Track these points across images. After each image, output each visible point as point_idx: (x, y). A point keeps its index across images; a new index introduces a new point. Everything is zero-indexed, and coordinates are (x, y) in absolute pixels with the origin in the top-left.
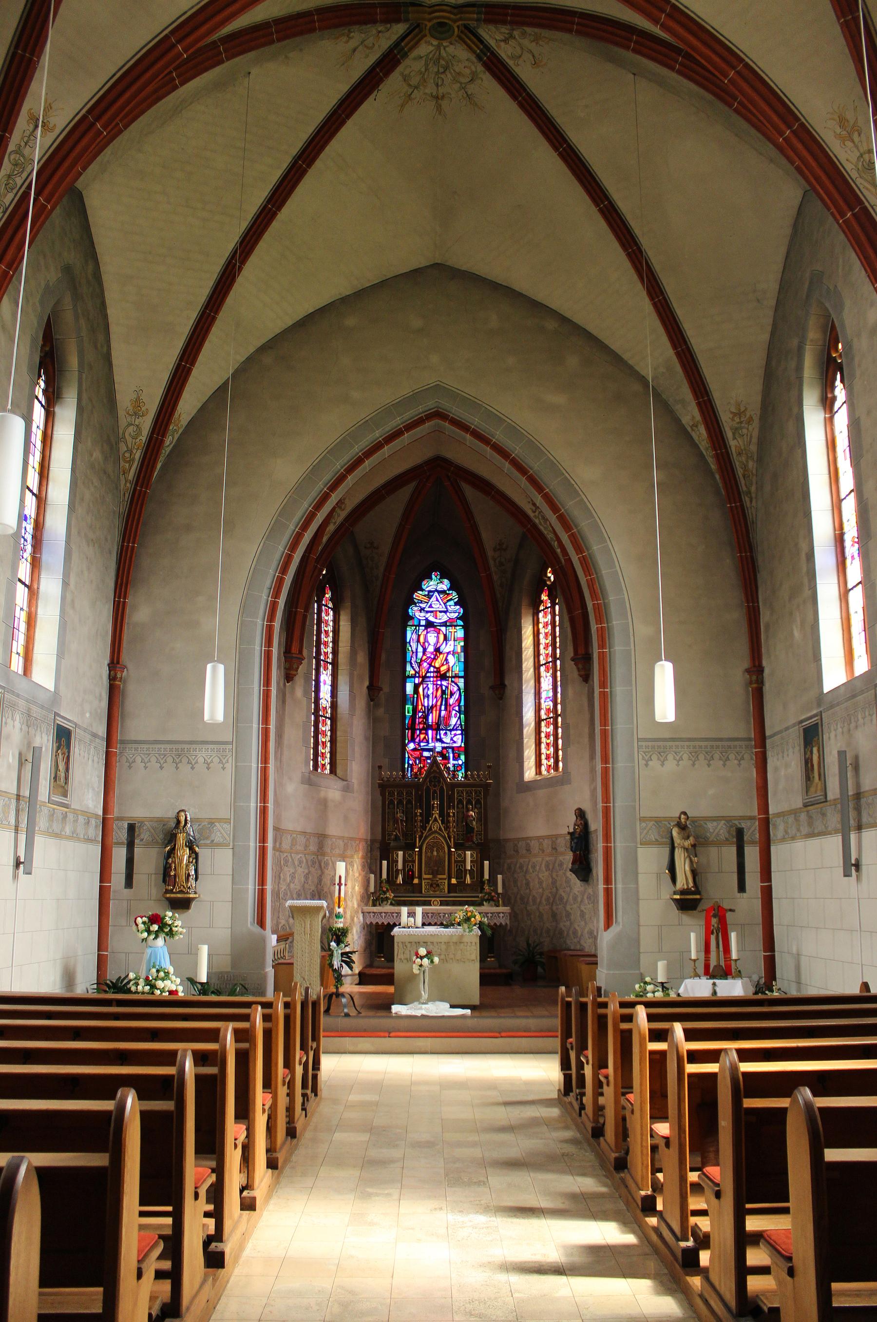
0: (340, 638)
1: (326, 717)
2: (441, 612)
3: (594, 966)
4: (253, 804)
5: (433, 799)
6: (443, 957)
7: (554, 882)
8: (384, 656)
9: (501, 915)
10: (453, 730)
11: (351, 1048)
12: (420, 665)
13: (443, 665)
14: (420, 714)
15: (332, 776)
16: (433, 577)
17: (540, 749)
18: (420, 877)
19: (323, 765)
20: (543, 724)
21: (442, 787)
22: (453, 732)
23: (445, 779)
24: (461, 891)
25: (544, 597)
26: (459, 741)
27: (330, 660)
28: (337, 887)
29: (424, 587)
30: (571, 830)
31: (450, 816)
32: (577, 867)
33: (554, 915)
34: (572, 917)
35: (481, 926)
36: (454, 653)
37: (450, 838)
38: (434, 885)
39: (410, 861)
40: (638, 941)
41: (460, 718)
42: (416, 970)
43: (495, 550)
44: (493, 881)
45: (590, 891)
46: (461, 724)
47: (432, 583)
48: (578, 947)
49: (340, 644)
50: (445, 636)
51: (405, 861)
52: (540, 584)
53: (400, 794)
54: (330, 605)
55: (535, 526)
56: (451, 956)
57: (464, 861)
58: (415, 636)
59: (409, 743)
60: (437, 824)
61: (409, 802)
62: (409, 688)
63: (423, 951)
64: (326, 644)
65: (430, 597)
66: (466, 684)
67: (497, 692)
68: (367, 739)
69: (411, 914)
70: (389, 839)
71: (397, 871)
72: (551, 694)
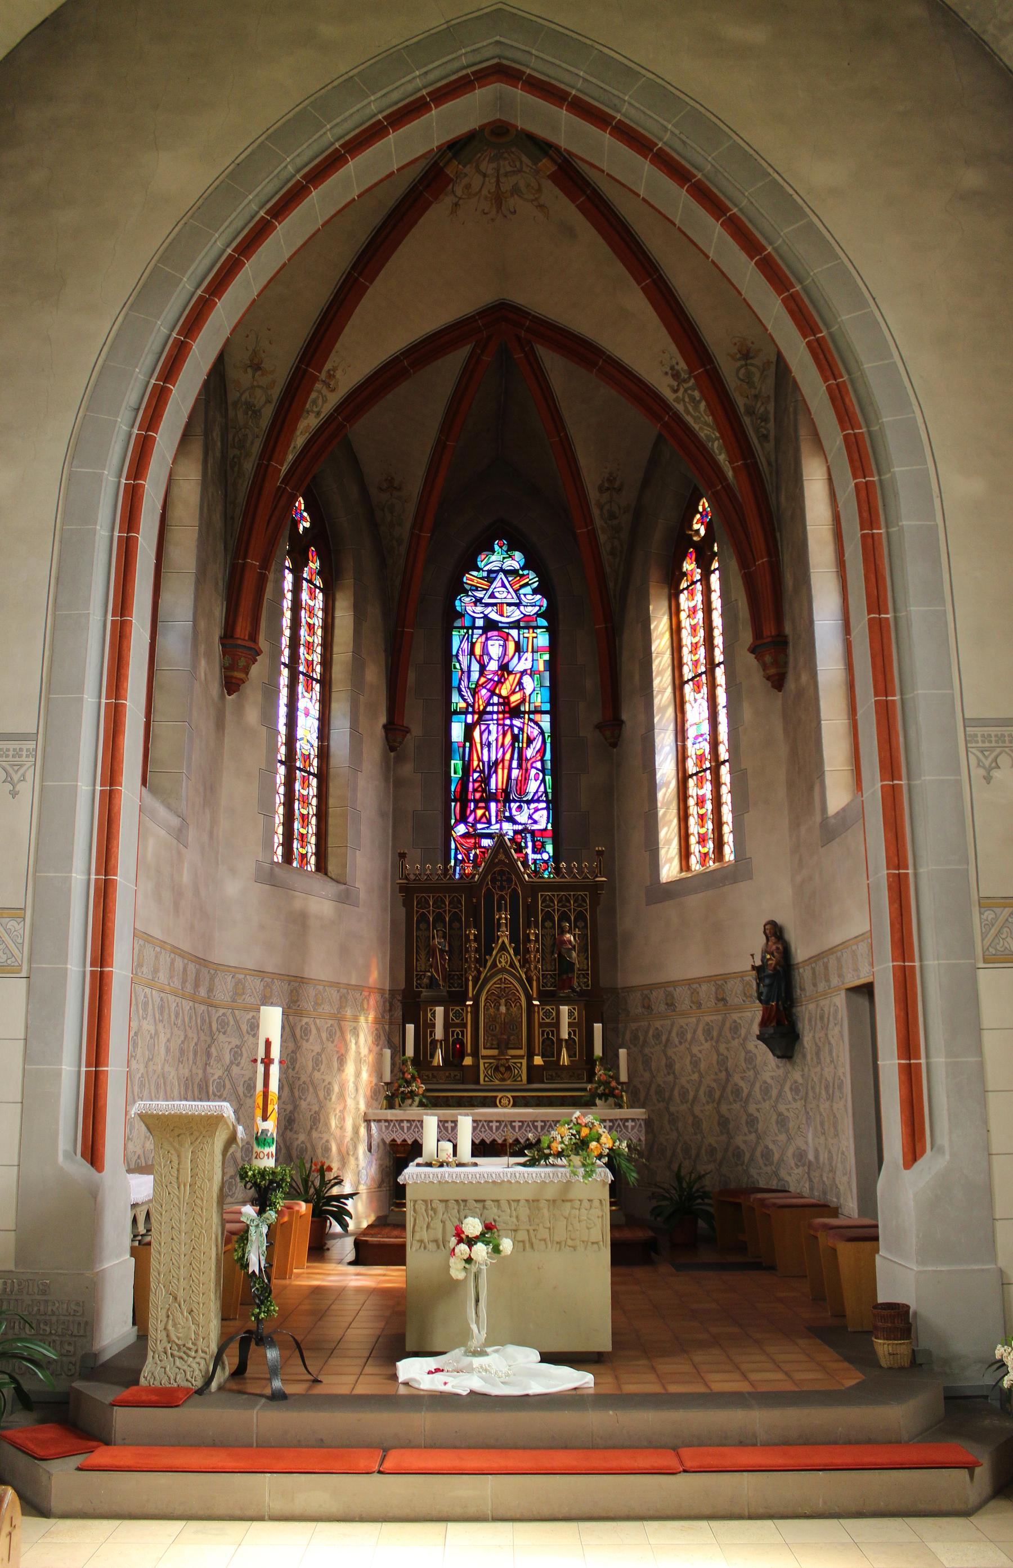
0: (336, 639)
1: (309, 773)
2: (509, 605)
3: (868, 1245)
4: (80, 875)
5: (499, 910)
6: (522, 1235)
7: (722, 1062)
8: (412, 677)
9: (630, 1124)
10: (532, 801)
11: (277, 1506)
12: (475, 693)
13: (514, 692)
14: (476, 775)
15: (320, 876)
16: (496, 547)
17: (687, 828)
18: (475, 1054)
19: (303, 856)
20: (691, 782)
21: (515, 890)
22: (533, 806)
23: (519, 876)
24: (551, 1079)
25: (688, 566)
26: (542, 820)
27: (317, 675)
28: (261, 1068)
29: (481, 565)
30: (758, 963)
31: (530, 941)
32: (771, 1030)
33: (724, 1123)
34: (760, 1126)
35: (612, 1161)
36: (532, 672)
37: (530, 980)
38: (502, 1069)
39: (457, 1025)
40: (989, 1189)
41: (543, 781)
42: (457, 1271)
43: (601, 489)
44: (610, 1059)
45: (797, 1076)
46: (546, 792)
47: (493, 558)
48: (774, 1184)
49: (336, 649)
50: (517, 644)
51: (447, 1025)
52: (681, 543)
53: (439, 903)
54: (318, 582)
55: (677, 417)
56: (544, 1233)
57: (557, 1024)
58: (465, 646)
59: (457, 823)
60: (507, 963)
61: (455, 917)
62: (457, 732)
63: (473, 1226)
64: (309, 646)
65: (491, 581)
66: (553, 723)
67: (608, 733)
68: (383, 815)
69: (448, 1131)
70: (419, 985)
71: (434, 1042)
72: (705, 728)
